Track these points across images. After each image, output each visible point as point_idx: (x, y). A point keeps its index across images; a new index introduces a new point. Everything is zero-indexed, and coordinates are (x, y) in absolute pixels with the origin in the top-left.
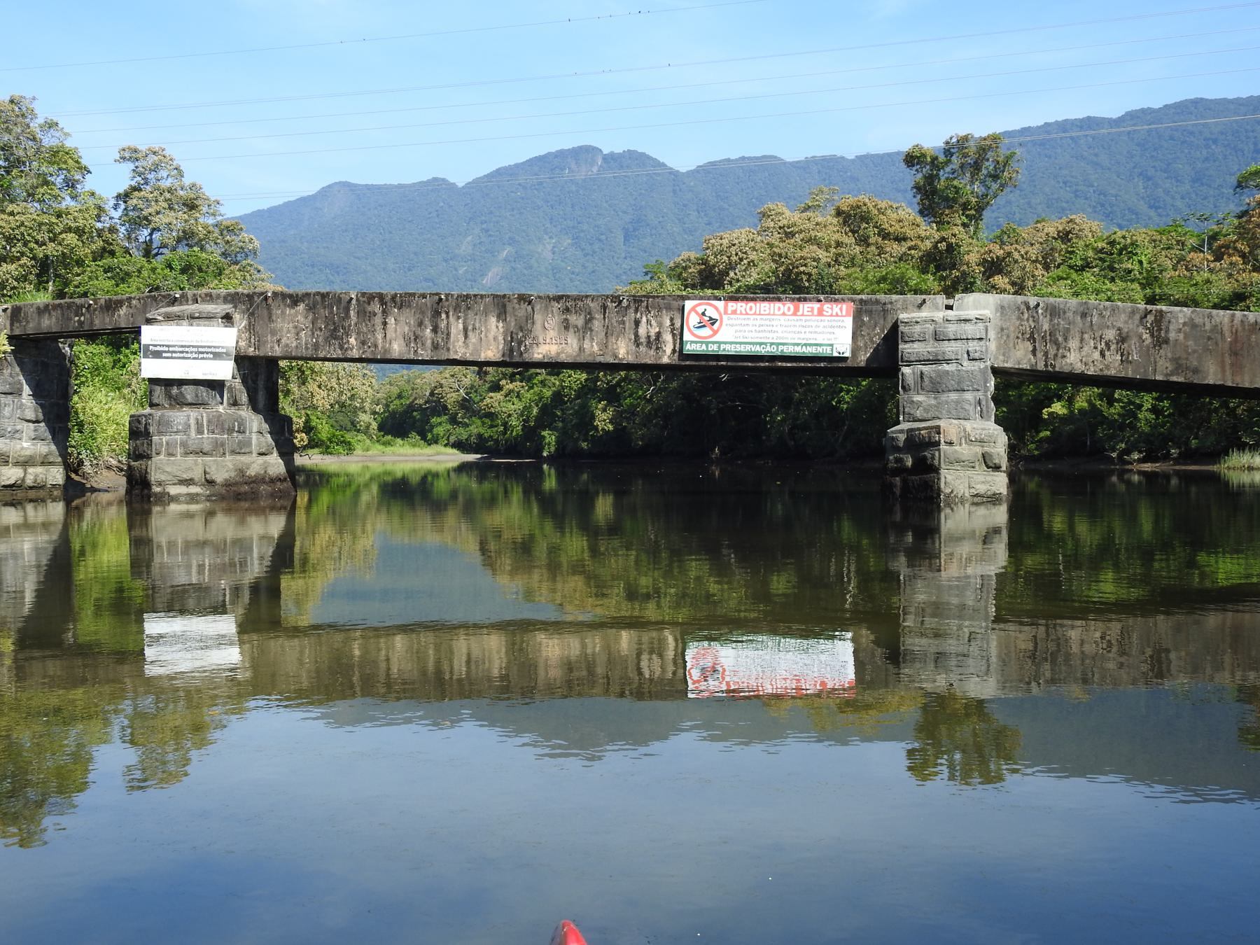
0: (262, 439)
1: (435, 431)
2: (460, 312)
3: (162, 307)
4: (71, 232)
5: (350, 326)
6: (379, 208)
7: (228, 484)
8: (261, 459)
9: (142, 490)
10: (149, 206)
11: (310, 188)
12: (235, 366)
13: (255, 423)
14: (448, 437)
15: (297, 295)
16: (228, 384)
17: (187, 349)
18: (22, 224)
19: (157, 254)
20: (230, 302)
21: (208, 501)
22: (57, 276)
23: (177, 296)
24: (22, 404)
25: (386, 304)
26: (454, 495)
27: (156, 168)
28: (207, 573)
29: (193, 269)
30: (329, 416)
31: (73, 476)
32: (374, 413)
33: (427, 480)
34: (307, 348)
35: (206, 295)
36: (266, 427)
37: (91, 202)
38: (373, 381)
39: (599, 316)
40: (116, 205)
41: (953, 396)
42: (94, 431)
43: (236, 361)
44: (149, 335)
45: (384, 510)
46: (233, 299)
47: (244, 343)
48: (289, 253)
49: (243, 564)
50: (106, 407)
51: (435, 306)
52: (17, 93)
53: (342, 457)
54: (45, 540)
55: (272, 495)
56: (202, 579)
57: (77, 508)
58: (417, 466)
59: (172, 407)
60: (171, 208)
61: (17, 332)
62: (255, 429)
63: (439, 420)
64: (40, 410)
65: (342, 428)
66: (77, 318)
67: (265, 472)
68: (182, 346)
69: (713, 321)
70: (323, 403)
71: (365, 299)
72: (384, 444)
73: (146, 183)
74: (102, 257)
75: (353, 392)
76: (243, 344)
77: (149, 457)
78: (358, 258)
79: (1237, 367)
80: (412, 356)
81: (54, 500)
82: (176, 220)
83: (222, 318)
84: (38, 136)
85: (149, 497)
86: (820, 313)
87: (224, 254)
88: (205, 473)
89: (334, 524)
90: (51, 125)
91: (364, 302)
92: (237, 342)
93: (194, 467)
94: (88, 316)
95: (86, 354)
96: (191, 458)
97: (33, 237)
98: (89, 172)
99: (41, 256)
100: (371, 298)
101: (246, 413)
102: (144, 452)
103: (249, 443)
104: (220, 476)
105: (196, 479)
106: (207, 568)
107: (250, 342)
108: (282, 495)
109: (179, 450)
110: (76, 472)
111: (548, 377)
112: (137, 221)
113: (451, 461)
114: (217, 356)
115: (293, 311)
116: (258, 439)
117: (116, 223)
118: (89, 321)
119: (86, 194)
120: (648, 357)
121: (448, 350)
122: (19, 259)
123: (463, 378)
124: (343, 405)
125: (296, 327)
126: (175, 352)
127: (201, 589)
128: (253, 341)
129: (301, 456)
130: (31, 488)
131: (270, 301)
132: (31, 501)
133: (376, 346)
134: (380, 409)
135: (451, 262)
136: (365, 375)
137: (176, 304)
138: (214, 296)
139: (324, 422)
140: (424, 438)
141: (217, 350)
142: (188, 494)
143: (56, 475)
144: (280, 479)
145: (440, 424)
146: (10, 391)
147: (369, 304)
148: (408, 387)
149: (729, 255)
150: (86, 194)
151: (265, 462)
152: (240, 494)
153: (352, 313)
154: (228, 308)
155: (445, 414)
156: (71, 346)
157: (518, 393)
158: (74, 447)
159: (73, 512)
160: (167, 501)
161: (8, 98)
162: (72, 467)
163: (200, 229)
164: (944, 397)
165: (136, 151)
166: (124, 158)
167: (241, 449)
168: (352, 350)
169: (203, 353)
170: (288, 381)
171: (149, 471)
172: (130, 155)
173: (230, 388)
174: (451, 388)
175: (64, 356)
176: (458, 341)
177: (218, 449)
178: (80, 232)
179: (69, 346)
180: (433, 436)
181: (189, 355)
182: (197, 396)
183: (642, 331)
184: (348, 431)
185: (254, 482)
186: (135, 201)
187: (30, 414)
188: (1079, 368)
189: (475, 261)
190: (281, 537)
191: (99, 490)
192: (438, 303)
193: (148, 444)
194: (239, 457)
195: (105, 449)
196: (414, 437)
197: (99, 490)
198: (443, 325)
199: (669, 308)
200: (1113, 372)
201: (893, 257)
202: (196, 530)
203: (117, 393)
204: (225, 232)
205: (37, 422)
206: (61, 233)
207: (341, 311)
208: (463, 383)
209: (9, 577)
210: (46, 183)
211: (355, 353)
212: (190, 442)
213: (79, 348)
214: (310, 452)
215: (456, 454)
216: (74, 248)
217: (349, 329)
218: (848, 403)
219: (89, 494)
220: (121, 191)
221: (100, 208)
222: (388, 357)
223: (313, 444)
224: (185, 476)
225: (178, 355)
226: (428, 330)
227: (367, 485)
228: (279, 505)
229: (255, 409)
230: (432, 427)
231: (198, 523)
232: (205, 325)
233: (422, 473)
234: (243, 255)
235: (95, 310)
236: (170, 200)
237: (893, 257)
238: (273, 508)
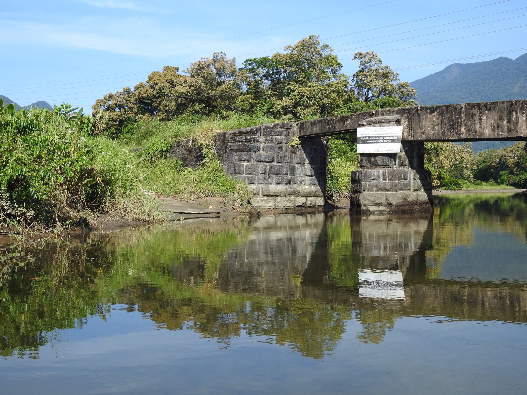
0: (416, 182)
1: (502, 178)
2: (524, 110)
3: (367, 118)
4: (334, 93)
5: (461, 122)
6: (473, 74)
7: (398, 205)
8: (415, 193)
9: (357, 209)
10: (367, 78)
11: (440, 68)
12: (402, 146)
13: (412, 174)
14: (509, 181)
15: (433, 107)
16: (398, 155)
17: (378, 138)
18: (314, 91)
19: (371, 100)
20: (399, 114)
21: (389, 214)
22: (328, 113)
23: (374, 112)
24: (305, 168)
25: (481, 109)
26: (512, 209)
27: (370, 61)
28: (388, 251)
29: (386, 105)
30: (450, 172)
31: (329, 201)
32: (472, 169)
33: (498, 202)
34: (438, 135)
35: (388, 111)
36: (417, 176)
37: (342, 79)
38: (472, 154)
40: (353, 79)
42: (338, 180)
43: (402, 143)
44: (361, 132)
45: (476, 217)
47: (406, 134)
48: (431, 98)
49: (406, 246)
50: (345, 169)
51: (509, 108)
52: (312, 34)
53: (457, 191)
54: (316, 231)
55: (421, 211)
56: (385, 254)
57: (331, 216)
58: (493, 195)
59: (371, 167)
60: (376, 79)
61: (302, 134)
62: (412, 177)
63: (504, 173)
64: (313, 171)
65: (456, 177)
66: (328, 126)
67: (417, 199)
68: (376, 137)
70: (447, 165)
71: (470, 107)
72: (477, 184)
73: (366, 68)
74: (347, 103)
75: (461, 160)
76: (405, 134)
78: (464, 98)
80: (496, 136)
81: (319, 213)
82: (379, 83)
83: (395, 122)
84: (321, 52)
85: (360, 212)
87: (400, 98)
88: (387, 200)
89: (452, 222)
90: (326, 46)
91: (469, 108)
92: (403, 134)
93: (382, 197)
94: (333, 125)
95: (334, 144)
96: (380, 193)
97: (318, 96)
98: (342, 66)
99: (322, 104)
100: (472, 106)
102: (358, 190)
103: (409, 185)
104: (394, 202)
105: (383, 203)
106: (388, 248)
107: (409, 133)
108: (426, 211)
110: (330, 199)
112: (361, 86)
113: (510, 192)
114: (393, 141)
115: (431, 116)
116: (413, 182)
117: (353, 87)
118: (334, 127)
119: (340, 75)
121: (517, 131)
122: (312, 106)
123: (516, 152)
124: (457, 166)
125: (433, 124)
126: (372, 140)
127: (385, 259)
128: (411, 132)
129: (436, 191)
130: (309, 207)
131: (419, 111)
132: (309, 213)
133: (476, 132)
134: (475, 167)
135: (509, 97)
136: (467, 151)
137: (373, 116)
138: (391, 111)
139: (448, 174)
140: (496, 181)
141: (393, 138)
142: (379, 211)
143: (320, 201)
144: (424, 203)
145: (505, 174)
146: (300, 162)
147: (472, 109)
148: (488, 157)
150: (340, 75)
151: (417, 194)
152: (404, 211)
153: (462, 115)
154: (398, 116)
155: (507, 170)
156: (327, 141)
158: (329, 188)
159: (328, 218)
160: (368, 214)
161: (308, 37)
162: (327, 197)
163: (389, 87)
165: (361, 54)
166: (356, 58)
167: (405, 187)
168: (462, 134)
169: (386, 140)
170: (430, 155)
171: (360, 199)
172: (359, 56)
173: (400, 157)
174: (510, 157)
175: (324, 145)
176: (523, 126)
177: (394, 188)
178: (337, 92)
179: (326, 140)
180: (501, 180)
181: (379, 141)
182: (383, 161)
184: (459, 179)
185: (412, 204)
186: (361, 77)
187: (308, 173)
189: (521, 95)
190: (426, 232)
191: (340, 208)
192: (511, 106)
193: (359, 186)
194: (404, 192)
195: (343, 188)
196: (492, 181)
197: (340, 208)
198: (514, 118)
202: (383, 229)
203: (352, 163)
204: (401, 88)
205: (312, 176)
206: (330, 94)
207: (457, 114)
208: (516, 154)
210: (324, 72)
211: (464, 136)
212: (380, 185)
213: (331, 142)
214: (441, 189)
215: (513, 189)
216: (335, 100)
217: (461, 124)
219: (336, 210)
220: (355, 73)
221: (346, 81)
222: (483, 137)
223: (442, 185)
224: (377, 202)
225: (374, 141)
226: (505, 122)
227: (469, 204)
228: (424, 216)
229: (412, 167)
230: (500, 176)
231: (384, 225)
232: (387, 126)
233: (496, 198)
234: (409, 97)
235: (336, 122)
236: (376, 75)
238: (421, 218)
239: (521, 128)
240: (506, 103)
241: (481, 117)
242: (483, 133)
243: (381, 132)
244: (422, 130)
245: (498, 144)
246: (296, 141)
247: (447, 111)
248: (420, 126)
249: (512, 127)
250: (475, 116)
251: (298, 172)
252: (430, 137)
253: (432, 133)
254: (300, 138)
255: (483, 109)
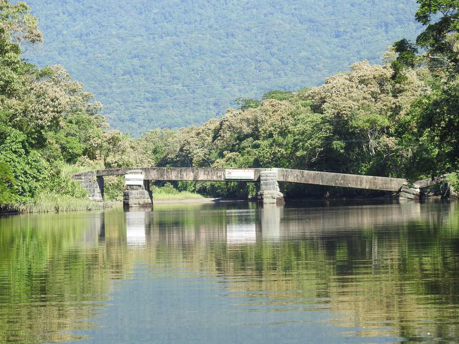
7: (142, 204)
13: (146, 192)
14: (195, 185)
39: (210, 172)
41: (269, 186)
46: (142, 169)
69: (230, 173)
77: (129, 200)
79: (314, 181)
86: (249, 171)
93: (137, 201)
96: (136, 200)
101: (144, 191)
104: (141, 203)
109: (134, 198)
111: (252, 150)
114: (140, 180)
120: (219, 179)
148: (161, 144)
149: (332, 92)
157: (234, 159)
164: (267, 186)
180: (183, 184)
183: (218, 175)
188: (290, 181)
198: (182, 174)
199: (223, 171)
200: (296, 182)
201: (378, 109)
209: (266, 172)
218: (365, 171)
237: (378, 109)
245: (178, 89)
246: (95, 178)
251: (95, 191)
254: (97, 177)
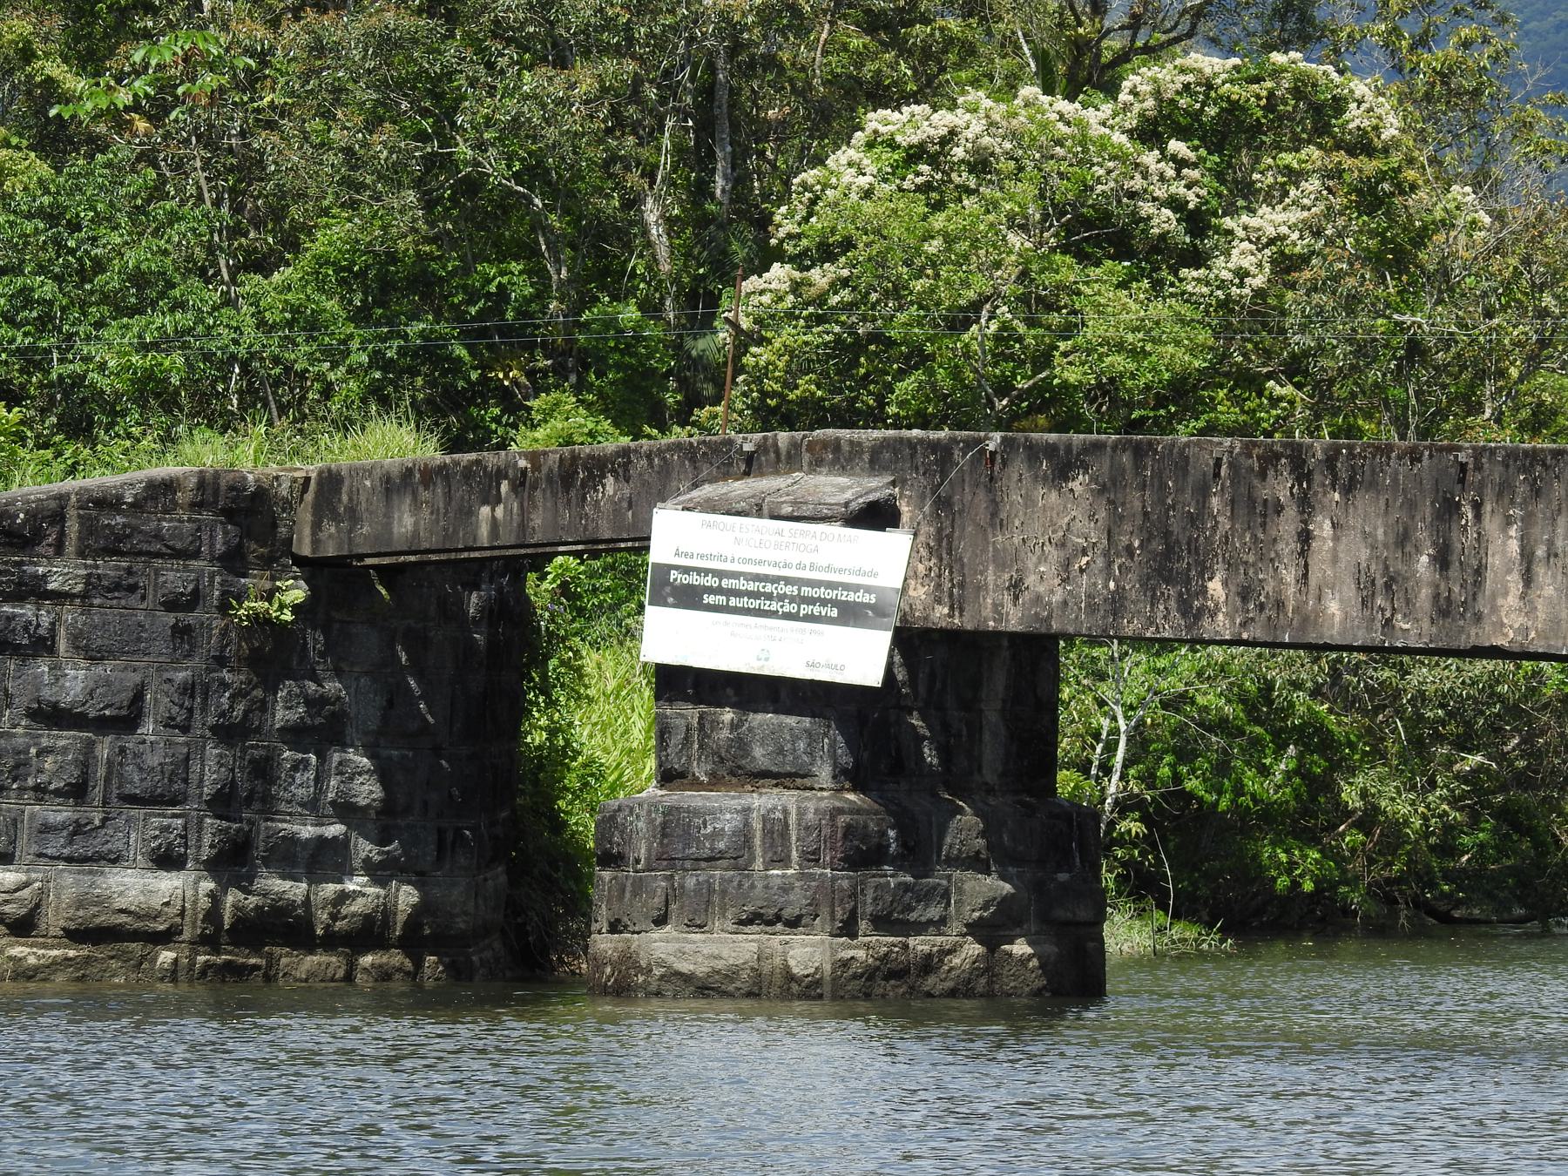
2: (1512, 502)
3: (712, 480)
17: (769, 588)
25: (1308, 477)
68: (757, 578)
107: (939, 586)
114: (851, 614)
133: (1280, 605)
138: (846, 448)
141: (852, 597)
147: (1263, 475)
168: (1213, 615)
169: (811, 601)
181: (775, 606)
207: (1188, 496)
225: (744, 602)
226: (1424, 559)
239: (1500, 601)
240: (1431, 456)
241: (1305, 522)
242: (1317, 616)
243: (793, 556)
244: (1007, 576)
247: (1137, 474)
248: (995, 549)
249: (1456, 589)
250: (1278, 513)
252: (1050, 616)
253: (1057, 598)
255: (1317, 478)
